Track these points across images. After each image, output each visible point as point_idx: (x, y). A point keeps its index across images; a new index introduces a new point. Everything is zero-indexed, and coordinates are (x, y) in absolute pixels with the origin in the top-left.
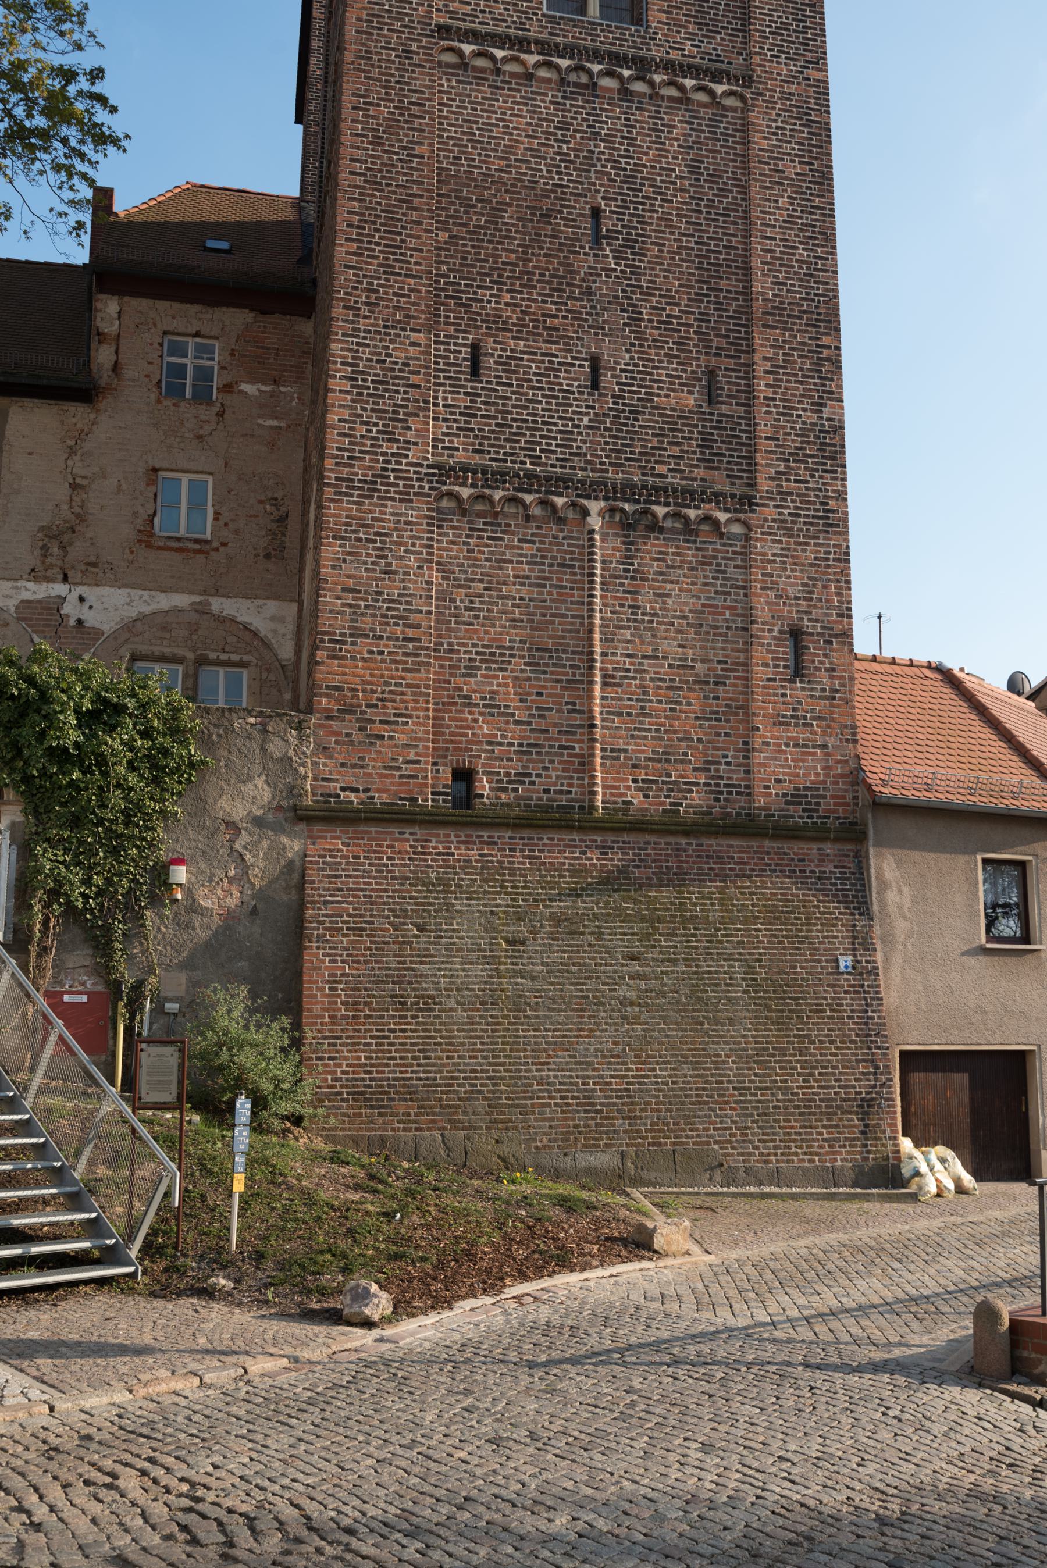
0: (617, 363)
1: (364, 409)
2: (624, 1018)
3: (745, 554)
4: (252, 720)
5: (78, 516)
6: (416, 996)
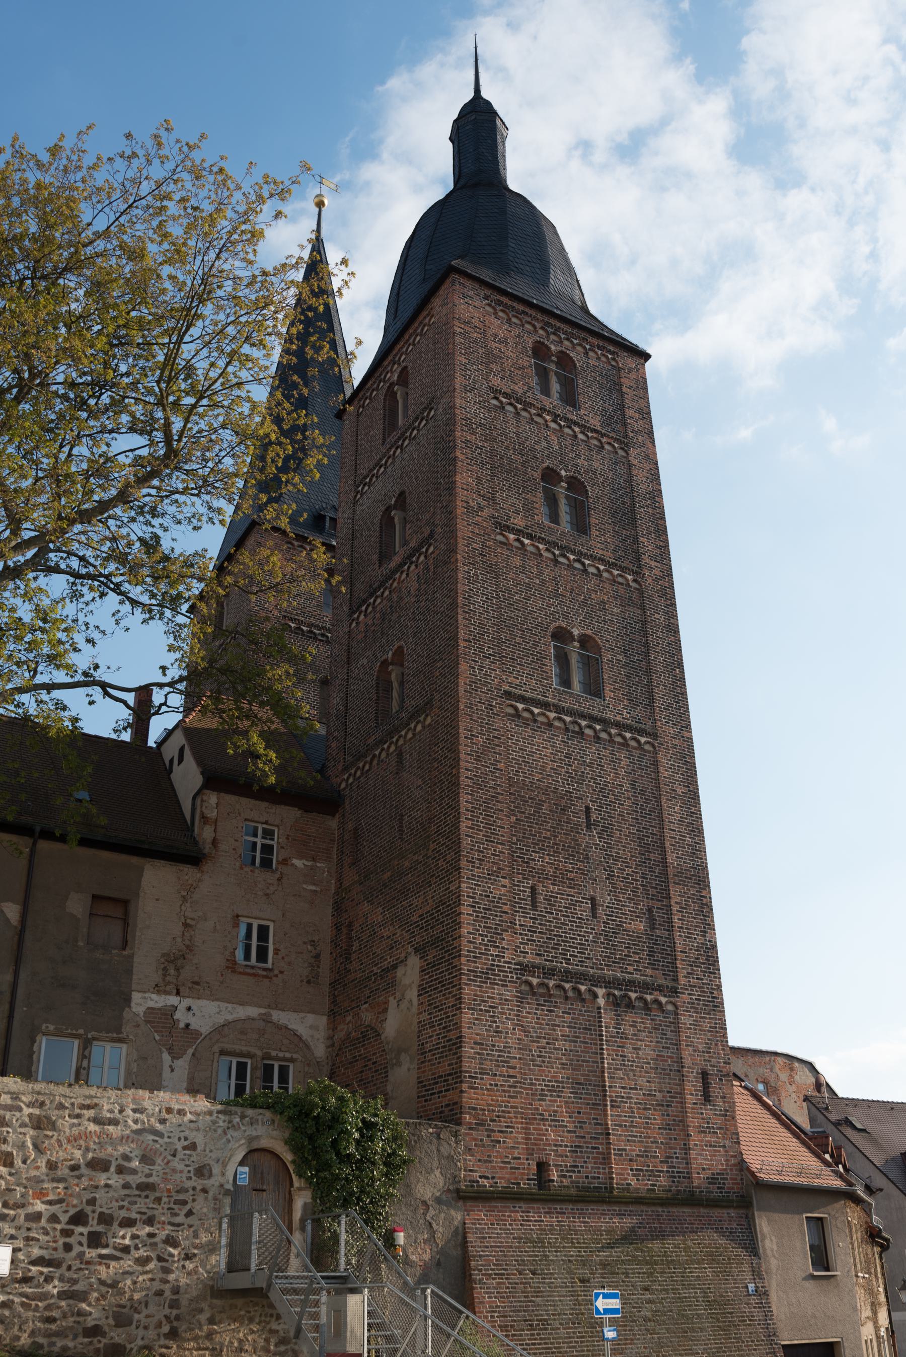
0: (604, 902)
1: (480, 926)
2: (647, 1330)
3: (676, 1023)
4: (431, 1130)
5: (188, 947)
6: (537, 1320)
